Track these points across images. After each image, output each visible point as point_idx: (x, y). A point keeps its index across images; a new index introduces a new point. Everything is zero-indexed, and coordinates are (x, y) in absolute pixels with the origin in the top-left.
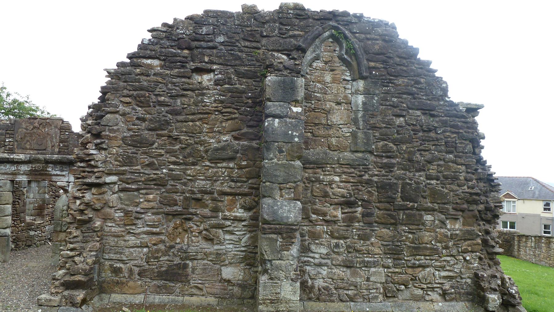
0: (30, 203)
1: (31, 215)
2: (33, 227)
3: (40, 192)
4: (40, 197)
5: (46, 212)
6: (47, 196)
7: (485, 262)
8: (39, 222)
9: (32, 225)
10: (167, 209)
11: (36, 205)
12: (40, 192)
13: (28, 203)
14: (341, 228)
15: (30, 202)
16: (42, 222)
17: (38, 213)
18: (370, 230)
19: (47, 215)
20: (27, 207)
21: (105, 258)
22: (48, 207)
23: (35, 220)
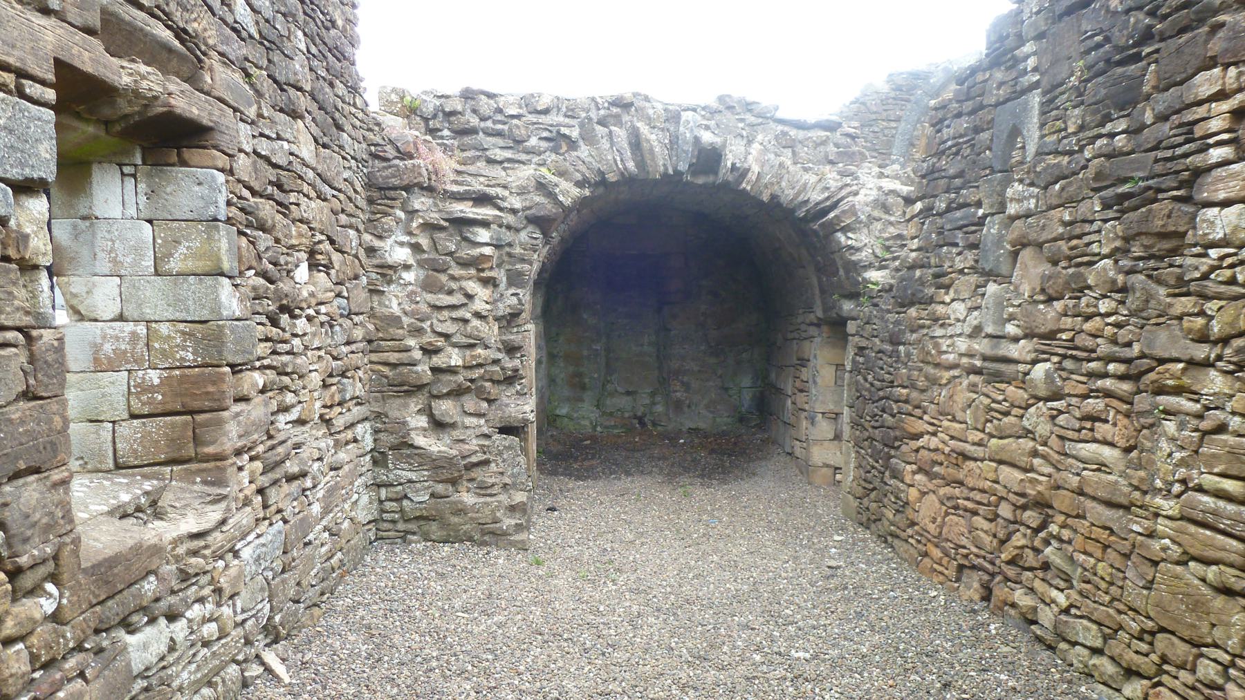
0: (101, 365)
1: (118, 467)
2: (150, 586)
3: (174, 265)
4: (177, 302)
5: (231, 435)
6: (230, 300)
7: (408, 350)
8: (190, 524)
9: (137, 568)
10: (370, 287)
11: (154, 377)
12: (174, 265)
13: (76, 357)
14: (810, 134)
15: (96, 348)
16: (214, 514)
17: (172, 441)
18: (941, 266)
19: (238, 453)
20: (72, 396)
21: (944, 381)
22: (246, 389)
23: (153, 508)
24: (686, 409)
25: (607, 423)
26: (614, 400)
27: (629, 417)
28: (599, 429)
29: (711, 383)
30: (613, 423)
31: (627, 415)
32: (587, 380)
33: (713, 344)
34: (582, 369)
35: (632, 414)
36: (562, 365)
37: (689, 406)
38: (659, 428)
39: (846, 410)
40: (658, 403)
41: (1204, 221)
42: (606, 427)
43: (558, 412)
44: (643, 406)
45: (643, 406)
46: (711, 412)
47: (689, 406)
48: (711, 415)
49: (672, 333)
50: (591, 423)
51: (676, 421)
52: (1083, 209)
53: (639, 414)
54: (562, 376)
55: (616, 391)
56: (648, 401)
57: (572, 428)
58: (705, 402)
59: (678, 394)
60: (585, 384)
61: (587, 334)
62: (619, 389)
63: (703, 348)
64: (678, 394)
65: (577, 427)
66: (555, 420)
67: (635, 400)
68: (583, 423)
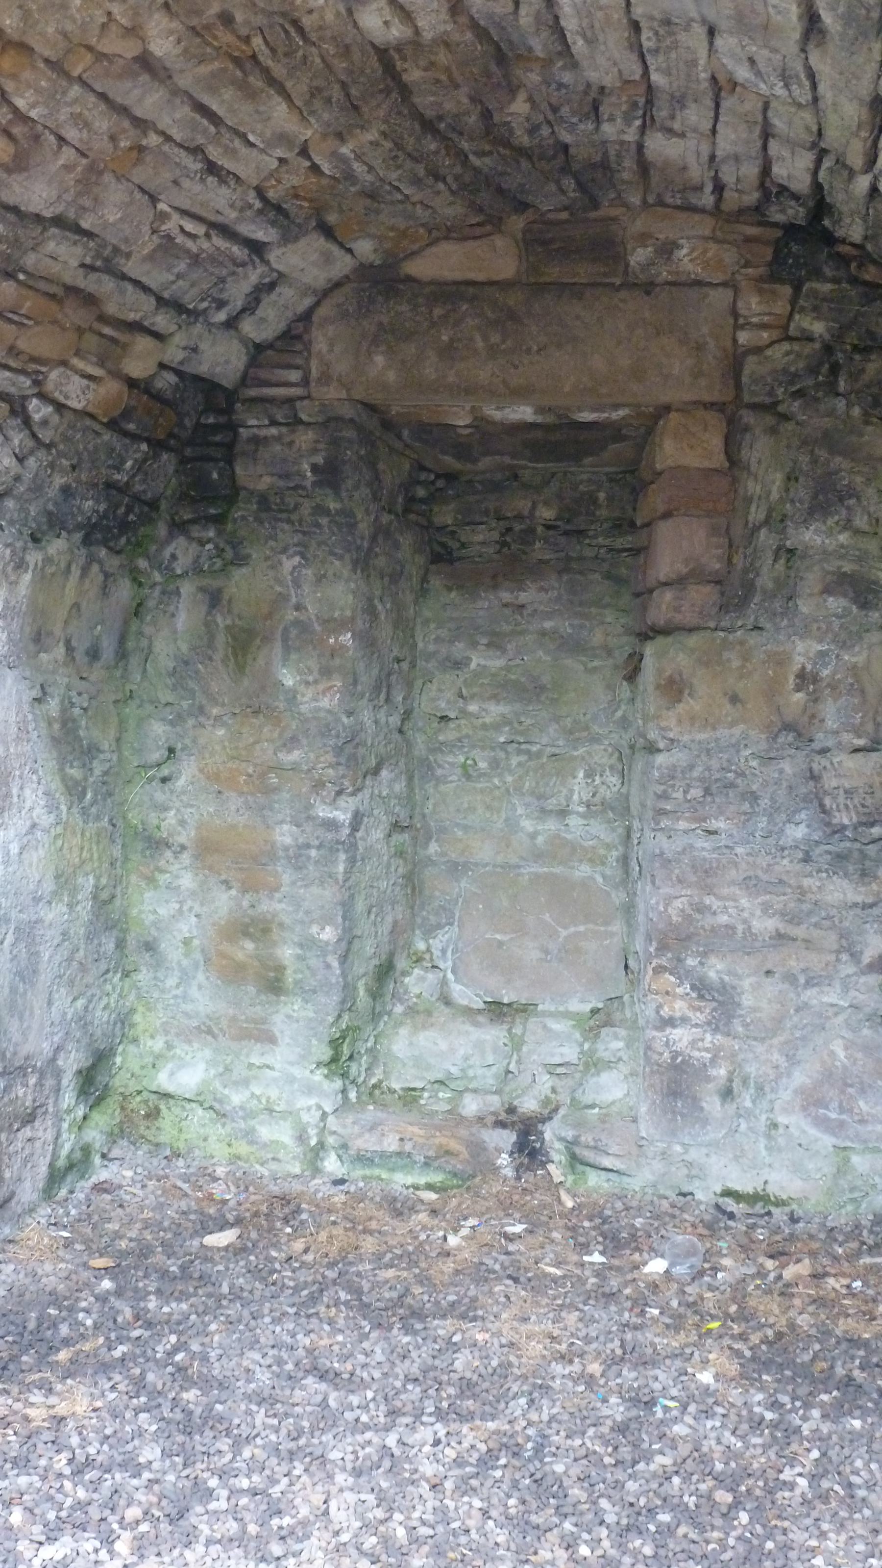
24: (712, 1104)
25: (367, 1143)
26: (425, 1039)
27: (480, 1119)
28: (332, 1164)
29: (832, 996)
30: (391, 1144)
31: (471, 1106)
32: (287, 953)
33: (844, 818)
34: (266, 906)
35: (495, 1102)
36: (187, 881)
37: (727, 1094)
38: (594, 1179)
39: (87, 1477)
40: (608, 1065)
41: (533, 130)
42: (363, 1159)
43: (163, 1080)
44: (551, 1069)
45: (551, 1069)
46: (823, 1123)
47: (727, 1094)
48: (828, 1141)
49: (660, 759)
50: (301, 1138)
51: (664, 1155)
52: (385, 143)
53: (529, 1105)
54: (186, 927)
55: (447, 1000)
56: (570, 1053)
57: (220, 1151)
58: (800, 1078)
59: (681, 1036)
60: (280, 969)
61: (295, 755)
62: (462, 994)
63: (797, 832)
64: (681, 1036)
65: (243, 1148)
66: (153, 1114)
67: (517, 1044)
68: (265, 1133)
